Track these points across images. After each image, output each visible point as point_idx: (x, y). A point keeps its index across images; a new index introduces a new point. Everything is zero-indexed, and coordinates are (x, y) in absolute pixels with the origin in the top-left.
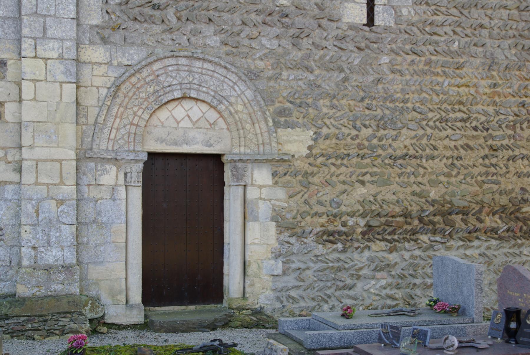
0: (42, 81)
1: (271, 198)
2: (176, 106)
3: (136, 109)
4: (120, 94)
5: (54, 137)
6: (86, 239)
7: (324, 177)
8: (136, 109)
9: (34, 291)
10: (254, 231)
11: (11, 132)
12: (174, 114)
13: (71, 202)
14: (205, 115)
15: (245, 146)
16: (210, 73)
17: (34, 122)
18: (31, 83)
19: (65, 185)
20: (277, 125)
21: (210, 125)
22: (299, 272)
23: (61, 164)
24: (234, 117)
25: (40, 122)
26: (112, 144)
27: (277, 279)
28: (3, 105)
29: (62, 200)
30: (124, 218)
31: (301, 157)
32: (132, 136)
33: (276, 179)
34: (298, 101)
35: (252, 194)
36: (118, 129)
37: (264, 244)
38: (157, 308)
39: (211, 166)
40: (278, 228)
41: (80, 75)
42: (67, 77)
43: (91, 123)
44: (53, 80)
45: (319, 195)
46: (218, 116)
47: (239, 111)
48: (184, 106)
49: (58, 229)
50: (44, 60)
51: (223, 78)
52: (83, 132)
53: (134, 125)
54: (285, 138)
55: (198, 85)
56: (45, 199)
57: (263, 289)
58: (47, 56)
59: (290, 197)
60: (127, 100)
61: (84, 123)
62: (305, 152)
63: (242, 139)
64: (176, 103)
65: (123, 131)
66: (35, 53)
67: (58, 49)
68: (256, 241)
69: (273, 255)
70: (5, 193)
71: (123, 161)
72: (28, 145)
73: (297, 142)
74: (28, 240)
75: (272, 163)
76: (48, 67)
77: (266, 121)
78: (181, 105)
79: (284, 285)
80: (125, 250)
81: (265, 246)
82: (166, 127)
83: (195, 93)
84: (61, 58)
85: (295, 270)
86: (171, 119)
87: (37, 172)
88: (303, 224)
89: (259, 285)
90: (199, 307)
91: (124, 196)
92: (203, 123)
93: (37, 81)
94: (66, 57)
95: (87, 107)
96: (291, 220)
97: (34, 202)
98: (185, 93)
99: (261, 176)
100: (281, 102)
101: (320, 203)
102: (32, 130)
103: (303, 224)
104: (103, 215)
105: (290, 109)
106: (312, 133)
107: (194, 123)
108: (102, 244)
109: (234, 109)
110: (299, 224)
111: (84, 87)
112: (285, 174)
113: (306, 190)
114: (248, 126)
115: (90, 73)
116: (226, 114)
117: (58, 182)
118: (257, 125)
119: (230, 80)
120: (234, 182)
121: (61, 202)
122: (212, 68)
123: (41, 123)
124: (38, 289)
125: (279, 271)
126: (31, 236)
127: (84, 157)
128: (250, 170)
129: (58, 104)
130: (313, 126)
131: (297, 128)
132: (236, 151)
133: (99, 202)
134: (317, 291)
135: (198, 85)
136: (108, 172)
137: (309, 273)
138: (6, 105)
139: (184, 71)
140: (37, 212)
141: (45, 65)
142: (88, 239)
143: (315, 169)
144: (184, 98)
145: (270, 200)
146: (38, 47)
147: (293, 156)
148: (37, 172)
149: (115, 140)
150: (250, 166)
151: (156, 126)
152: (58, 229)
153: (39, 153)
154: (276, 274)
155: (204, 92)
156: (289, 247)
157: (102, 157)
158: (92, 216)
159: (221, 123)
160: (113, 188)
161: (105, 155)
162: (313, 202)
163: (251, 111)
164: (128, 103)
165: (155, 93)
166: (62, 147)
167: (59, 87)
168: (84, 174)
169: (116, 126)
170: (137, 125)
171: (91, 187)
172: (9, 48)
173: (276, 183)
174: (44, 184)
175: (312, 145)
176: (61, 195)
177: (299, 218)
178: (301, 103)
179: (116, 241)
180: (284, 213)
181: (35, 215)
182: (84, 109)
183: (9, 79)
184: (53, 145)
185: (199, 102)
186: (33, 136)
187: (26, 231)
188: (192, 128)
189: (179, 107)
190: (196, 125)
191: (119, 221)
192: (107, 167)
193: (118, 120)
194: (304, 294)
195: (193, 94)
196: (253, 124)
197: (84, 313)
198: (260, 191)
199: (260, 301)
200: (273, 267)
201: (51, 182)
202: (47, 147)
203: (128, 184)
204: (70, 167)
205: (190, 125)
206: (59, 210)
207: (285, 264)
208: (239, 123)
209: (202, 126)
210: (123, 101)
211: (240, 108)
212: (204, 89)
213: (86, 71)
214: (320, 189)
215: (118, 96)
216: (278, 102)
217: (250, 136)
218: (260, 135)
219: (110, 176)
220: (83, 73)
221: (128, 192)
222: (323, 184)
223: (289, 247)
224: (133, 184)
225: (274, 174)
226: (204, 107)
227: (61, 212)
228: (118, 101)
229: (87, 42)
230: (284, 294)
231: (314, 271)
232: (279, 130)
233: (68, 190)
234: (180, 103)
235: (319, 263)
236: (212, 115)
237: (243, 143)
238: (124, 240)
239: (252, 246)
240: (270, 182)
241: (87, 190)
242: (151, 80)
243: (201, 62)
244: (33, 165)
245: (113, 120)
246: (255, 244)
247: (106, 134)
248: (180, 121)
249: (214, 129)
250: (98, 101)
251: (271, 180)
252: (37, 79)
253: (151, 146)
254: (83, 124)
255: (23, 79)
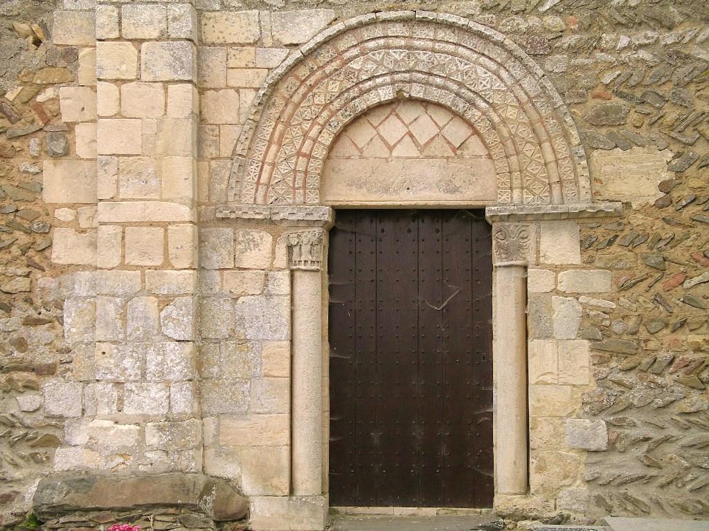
0: (131, 81)
1: (580, 291)
2: (387, 118)
3: (306, 126)
4: (279, 101)
5: (153, 182)
6: (215, 370)
7: (699, 247)
8: (306, 126)
9: (114, 464)
10: (543, 354)
11: (86, 177)
12: (382, 134)
13: (184, 299)
14: (444, 130)
15: (522, 188)
16: (451, 48)
17: (118, 156)
18: (113, 86)
19: (173, 268)
20: (589, 144)
21: (454, 150)
22: (645, 446)
23: (166, 230)
24: (499, 132)
25: (128, 156)
26: (262, 193)
27: (595, 458)
28: (73, 129)
29: (167, 296)
30: (286, 330)
31: (644, 209)
32: (300, 176)
33: (591, 252)
34: (638, 93)
35: (539, 282)
36: (273, 165)
37: (564, 384)
38: (360, 509)
39: (463, 233)
40: (594, 353)
41: (205, 68)
42: (176, 72)
43: (226, 155)
44: (151, 78)
45: (687, 285)
46: (470, 132)
47: (508, 119)
48: (401, 116)
49: (161, 351)
50: (136, 43)
51: (475, 56)
52: (212, 173)
53: (305, 155)
54: (608, 169)
55: (426, 73)
56: (136, 295)
57: (566, 477)
58: (140, 36)
59: (623, 288)
60: (290, 108)
61: (214, 156)
62: (652, 193)
63: (516, 174)
64: (388, 111)
65: (283, 168)
66: (120, 30)
67: (160, 22)
68: (548, 378)
69: (587, 409)
70: (76, 286)
71: (285, 224)
72: (108, 197)
73: (636, 175)
74: (107, 368)
75: (581, 221)
76: (143, 56)
77: (566, 136)
78: (397, 115)
79: (616, 472)
80: (287, 391)
81: (569, 388)
82: (367, 158)
83: (418, 89)
84: (164, 37)
85: (637, 442)
86: (378, 142)
87: (123, 246)
88: (652, 345)
89: (558, 470)
90: (442, 511)
91: (285, 289)
92: (439, 147)
93: (124, 81)
94: (173, 36)
95: (218, 125)
96: (625, 337)
97: (118, 300)
98: (401, 90)
99: (559, 247)
100: (598, 96)
101: (688, 301)
102: (114, 170)
103: (652, 345)
104: (247, 325)
105: (618, 110)
106: (671, 155)
107: (422, 148)
108: (247, 379)
109: (499, 116)
110: (643, 345)
111: (214, 89)
112: (610, 243)
113: (657, 275)
114: (529, 149)
115: (224, 64)
116: (482, 127)
117: (159, 263)
118: (546, 145)
119: (490, 59)
120: (501, 259)
121: (165, 301)
122: (453, 39)
123: (131, 158)
124: (121, 460)
125: (601, 442)
126: (112, 361)
127: (211, 220)
128: (532, 236)
129: (160, 122)
130: (672, 142)
131: (635, 147)
132: (504, 198)
133: (240, 301)
134: (691, 491)
135: (426, 73)
136: (256, 245)
137: (670, 450)
138: (78, 129)
139: (400, 47)
140: (124, 317)
141: (136, 52)
142: (221, 370)
143: (679, 231)
144: (399, 100)
145: (577, 296)
146: (124, 20)
147: (627, 205)
148: (123, 246)
149: (268, 185)
150: (532, 228)
151: (349, 158)
152: (161, 351)
153: (128, 212)
154: (593, 448)
155: (438, 87)
156: (623, 392)
157: (246, 217)
158: (224, 330)
159: (475, 146)
160: (266, 275)
161: (251, 215)
162: (675, 299)
163: (535, 116)
164: (292, 115)
165: (342, 93)
166: (167, 200)
167: (163, 91)
168: (214, 249)
169: (269, 159)
170: (309, 156)
171: (226, 272)
172: (82, 26)
173: (590, 262)
174: (137, 267)
175: (671, 181)
176: (166, 286)
177: (644, 334)
178: (644, 95)
179: (272, 373)
180: (607, 323)
181: (119, 324)
182: (213, 130)
183: (82, 82)
184: (152, 196)
185: (431, 110)
186: (117, 182)
187: (104, 353)
188: (418, 158)
189: (393, 119)
190: (426, 152)
191: (277, 336)
192: (255, 234)
193: (274, 148)
194: (664, 496)
195: (417, 91)
196: (540, 144)
197: (203, 506)
198: (556, 277)
199: (561, 502)
200: (586, 433)
201: (149, 263)
202: (141, 200)
203: (294, 267)
204: (184, 236)
205: (414, 152)
206: (163, 314)
207: (614, 429)
208: (509, 143)
209: (437, 153)
210: (283, 112)
211: (511, 113)
212: (438, 80)
213: (216, 60)
214: (692, 273)
215: (274, 104)
216: (594, 97)
217: (533, 168)
218: (553, 165)
219: (260, 251)
220: (210, 64)
221: (295, 281)
222: (697, 261)
223: (623, 392)
224: (303, 267)
225: (586, 245)
226: (442, 118)
227: (165, 318)
228: (274, 112)
229: (218, 8)
230: (614, 491)
231: (683, 447)
232: (595, 153)
233: (181, 278)
234: (393, 110)
235: (693, 430)
236: (457, 132)
237: (516, 183)
238: (287, 372)
239: (540, 388)
240: (576, 259)
241: (218, 279)
242: (336, 70)
243: (432, 27)
244: (116, 234)
245: (264, 148)
246: (546, 384)
247: (252, 174)
248: (395, 146)
249: (461, 157)
250: (239, 114)
251: (579, 256)
252: (124, 78)
253: (339, 194)
254: (212, 159)
255: (100, 80)
